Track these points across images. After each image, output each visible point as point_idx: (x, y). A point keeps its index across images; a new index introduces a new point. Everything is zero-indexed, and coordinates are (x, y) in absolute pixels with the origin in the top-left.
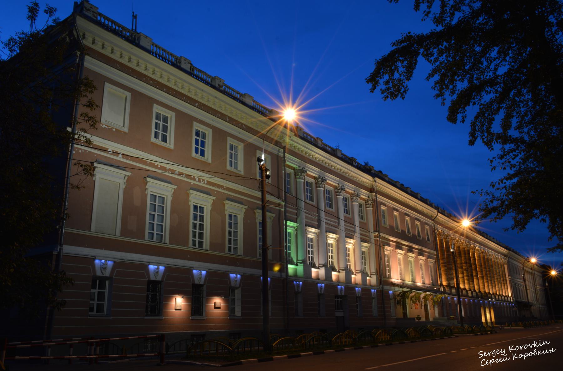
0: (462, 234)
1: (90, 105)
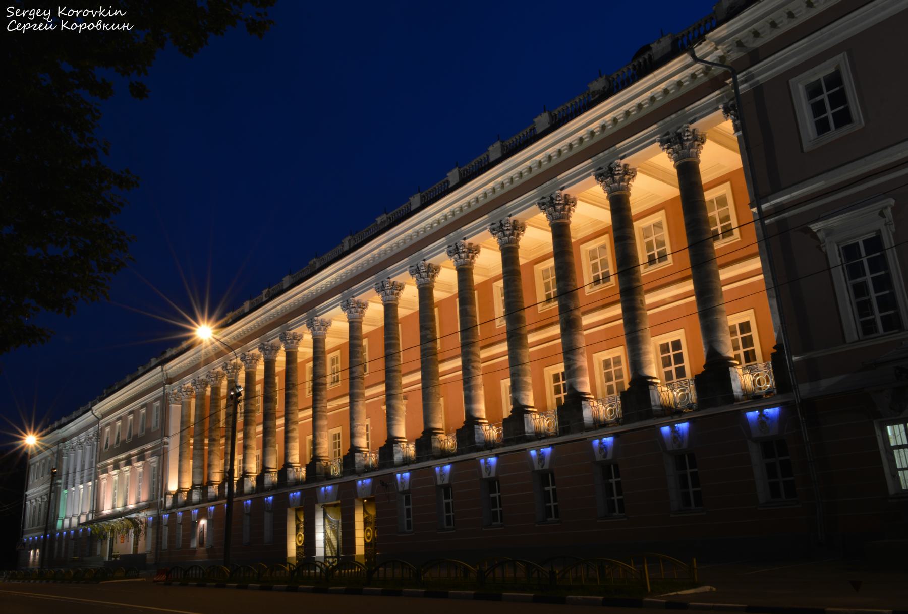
0: (219, 354)
1: (411, 239)
